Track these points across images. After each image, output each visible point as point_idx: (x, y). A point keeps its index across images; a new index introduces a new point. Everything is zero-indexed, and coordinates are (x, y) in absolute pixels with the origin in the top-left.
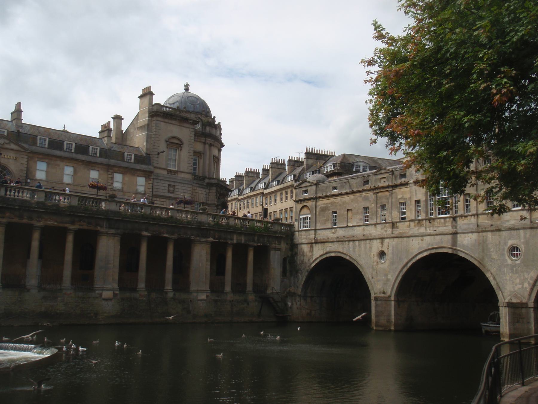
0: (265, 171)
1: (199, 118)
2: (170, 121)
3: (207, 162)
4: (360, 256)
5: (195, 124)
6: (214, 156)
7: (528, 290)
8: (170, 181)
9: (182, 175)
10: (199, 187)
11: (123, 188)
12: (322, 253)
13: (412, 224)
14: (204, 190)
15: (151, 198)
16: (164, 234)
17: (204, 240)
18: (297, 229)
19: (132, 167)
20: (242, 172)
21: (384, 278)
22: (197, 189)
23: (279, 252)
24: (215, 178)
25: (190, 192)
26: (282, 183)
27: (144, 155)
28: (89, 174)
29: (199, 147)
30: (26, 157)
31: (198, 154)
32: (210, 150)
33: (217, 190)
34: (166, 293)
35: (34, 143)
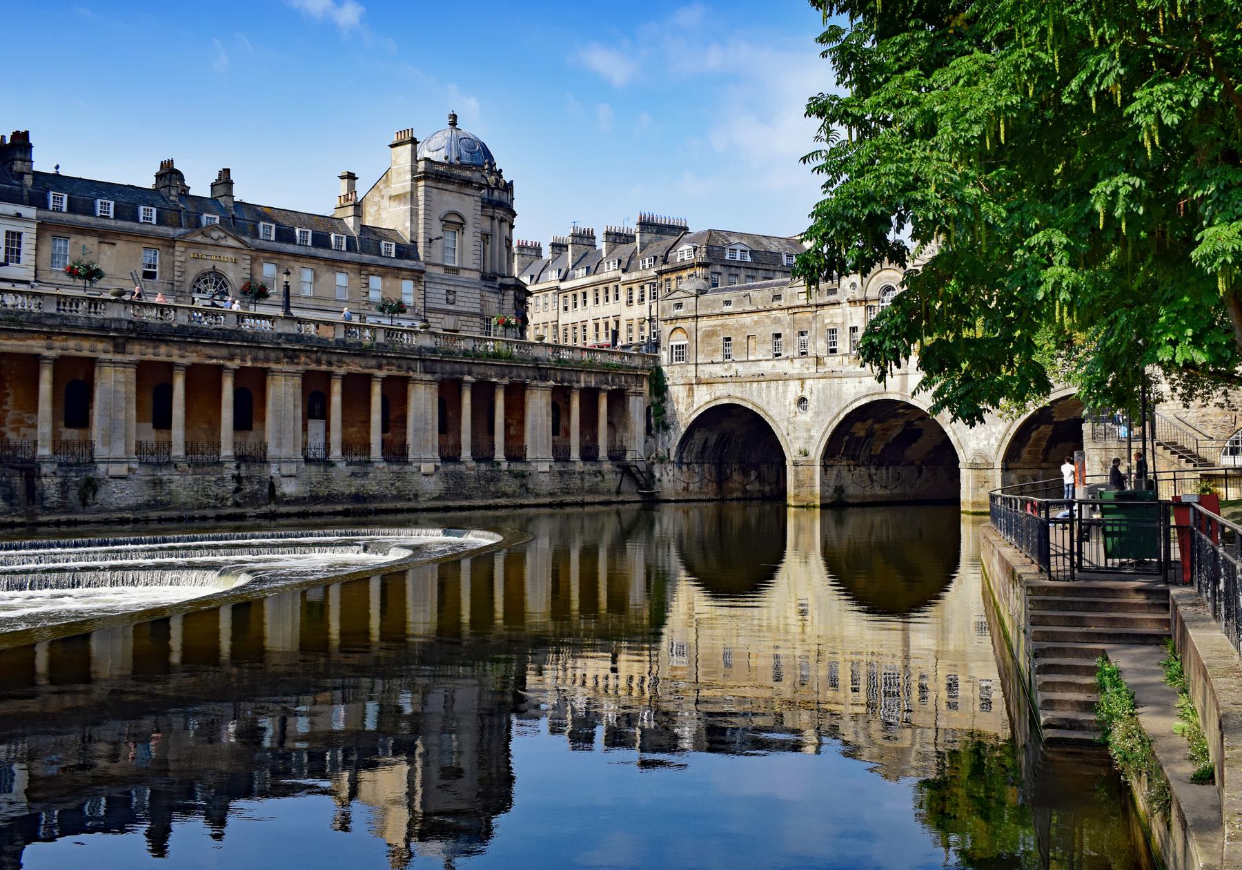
0: (559, 247)
2: (445, 187)
4: (768, 403)
7: (996, 446)
13: (846, 359)
16: (491, 377)
19: (393, 265)
25: (478, 301)
27: (409, 243)
30: (249, 257)
31: (485, 237)
34: (499, 464)
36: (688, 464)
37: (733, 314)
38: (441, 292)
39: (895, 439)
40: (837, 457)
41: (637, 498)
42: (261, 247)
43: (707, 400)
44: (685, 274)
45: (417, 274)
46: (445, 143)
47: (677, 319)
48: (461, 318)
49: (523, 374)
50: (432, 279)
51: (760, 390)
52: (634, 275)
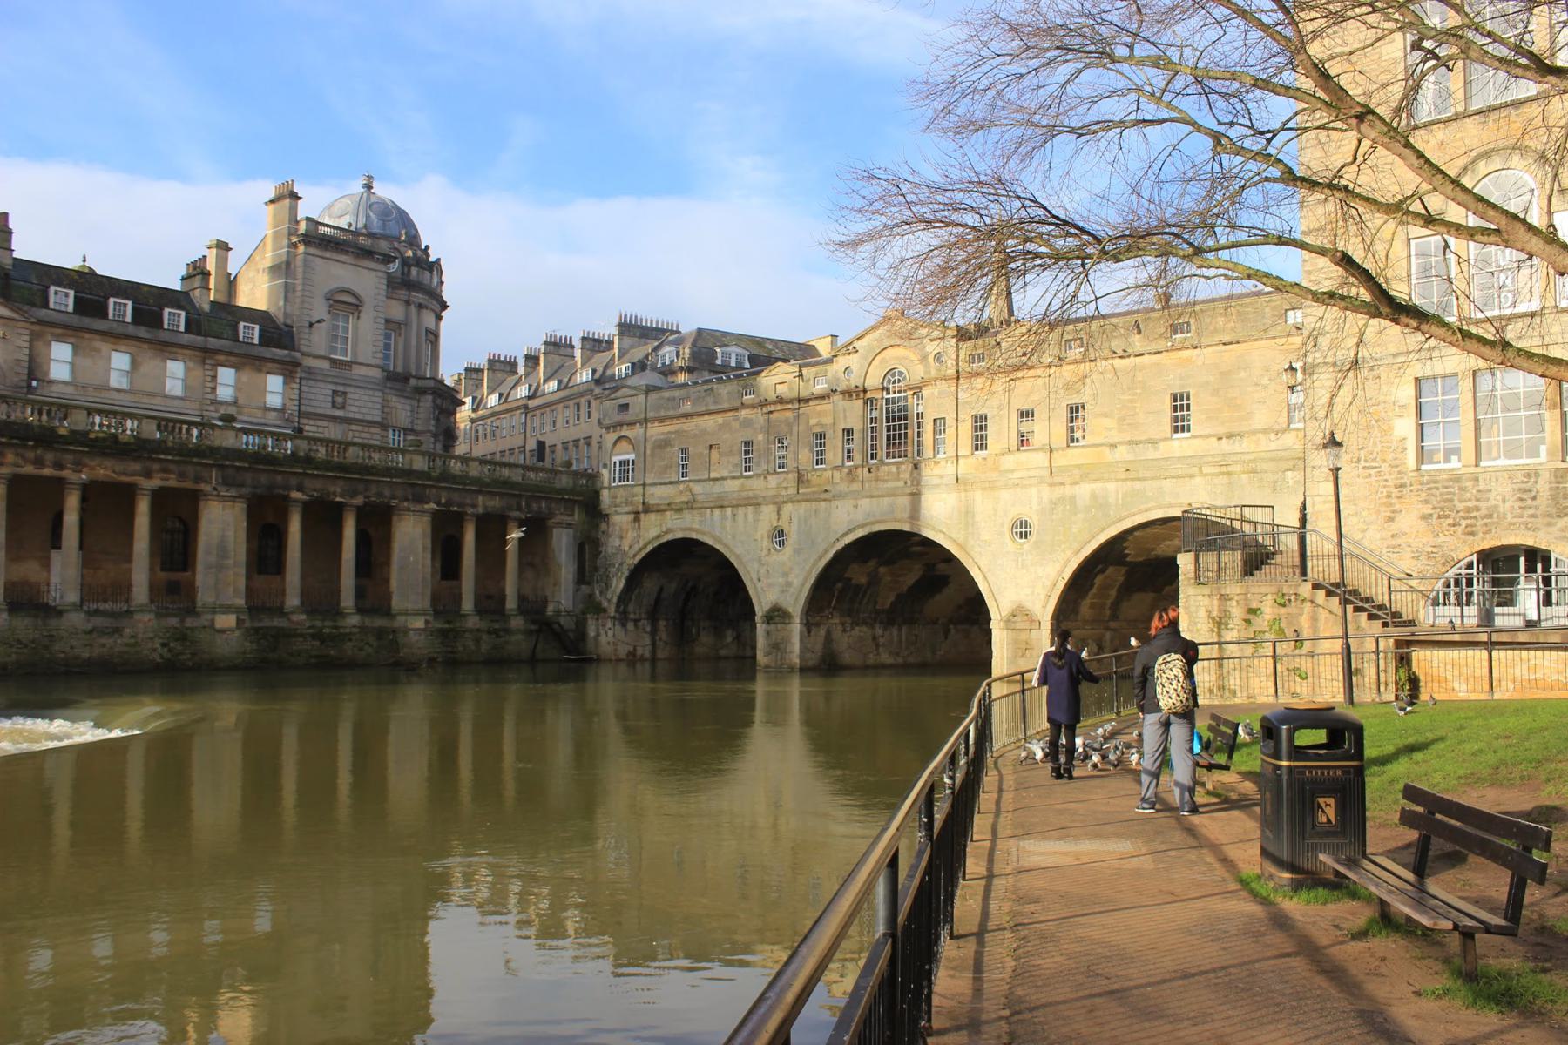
0: (532, 360)
1: (396, 249)
2: (335, 256)
3: (414, 342)
5: (389, 262)
6: (428, 331)
7: (1042, 597)
8: (336, 384)
9: (363, 371)
11: (236, 398)
13: (837, 474)
14: (409, 401)
15: (297, 419)
17: (418, 507)
18: (606, 484)
20: (481, 361)
21: (780, 580)
22: (394, 399)
24: (428, 376)
25: (379, 406)
26: (566, 388)
29: (397, 311)
30: (27, 332)
32: (419, 314)
33: (434, 401)
35: (1401, 617)
38: (324, 392)
39: (910, 589)
40: (827, 612)
42: (47, 319)
45: (290, 368)
46: (351, 207)
48: (353, 427)
49: (387, 492)
50: (310, 372)
51: (724, 518)
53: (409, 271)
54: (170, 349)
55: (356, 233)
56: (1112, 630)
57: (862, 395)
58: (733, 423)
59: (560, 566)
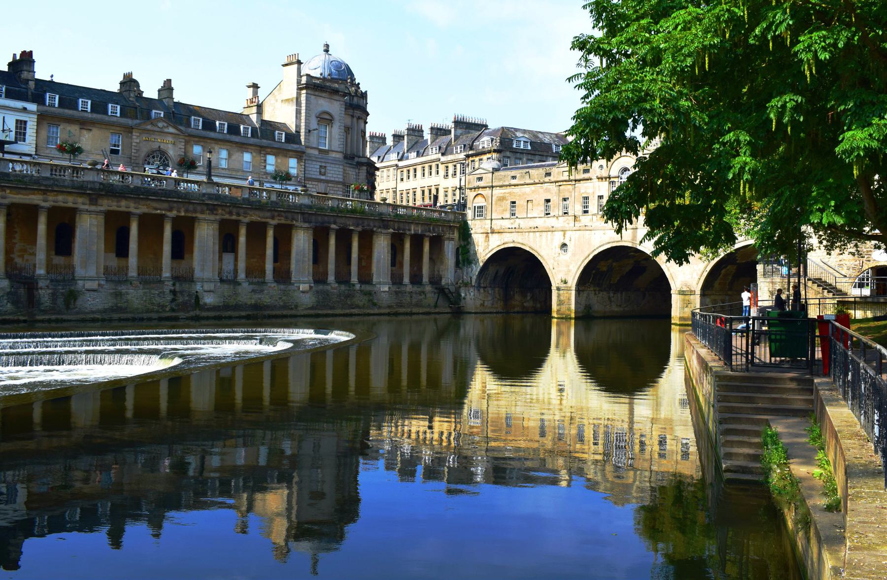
0: (398, 137)
4: (540, 247)
9: (334, 155)
10: (349, 167)
12: (499, 243)
13: (594, 217)
17: (385, 231)
23: (453, 242)
25: (341, 173)
28: (243, 156)
31: (347, 130)
33: (367, 169)
34: (354, 285)
36: (484, 288)
37: (518, 185)
38: (316, 166)
40: (587, 285)
41: (449, 310)
42: (192, 134)
43: (499, 244)
44: (485, 157)
47: (479, 188)
48: (330, 185)
49: (372, 224)
52: (450, 157)
53: (353, 99)
54: (245, 146)
55: (324, 79)
56: (729, 295)
57: (608, 179)
58: (540, 190)
59: (448, 259)
